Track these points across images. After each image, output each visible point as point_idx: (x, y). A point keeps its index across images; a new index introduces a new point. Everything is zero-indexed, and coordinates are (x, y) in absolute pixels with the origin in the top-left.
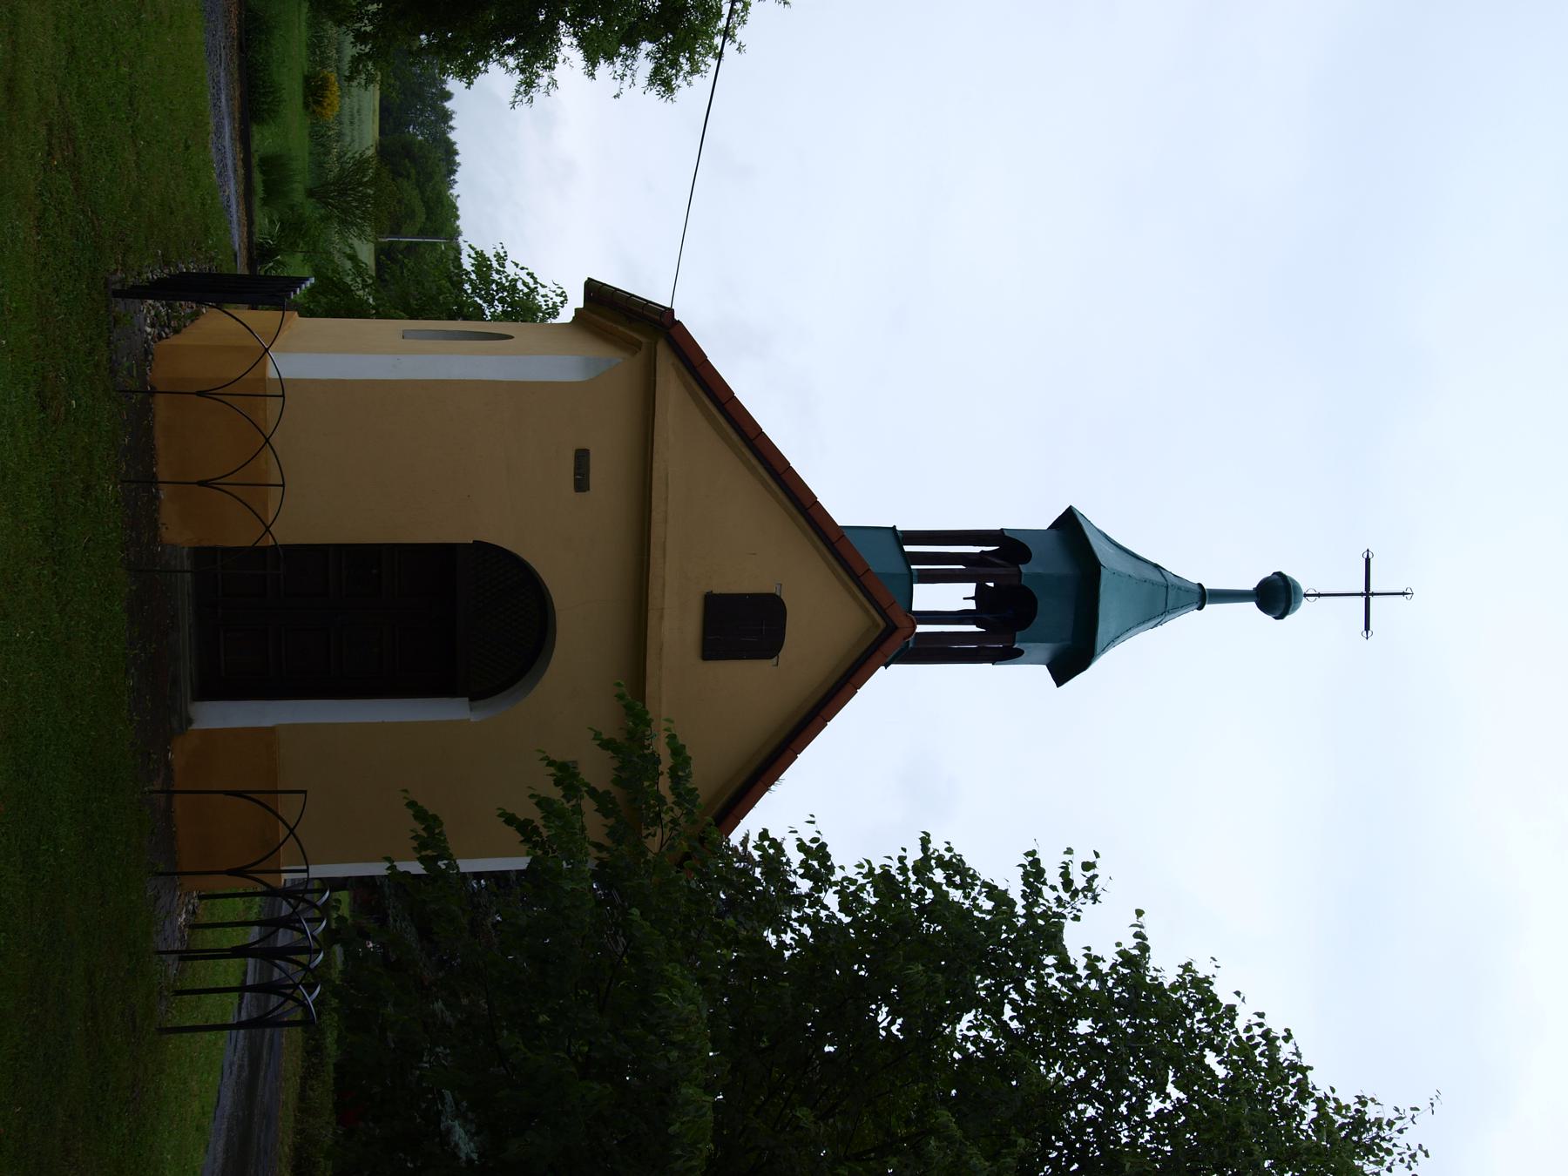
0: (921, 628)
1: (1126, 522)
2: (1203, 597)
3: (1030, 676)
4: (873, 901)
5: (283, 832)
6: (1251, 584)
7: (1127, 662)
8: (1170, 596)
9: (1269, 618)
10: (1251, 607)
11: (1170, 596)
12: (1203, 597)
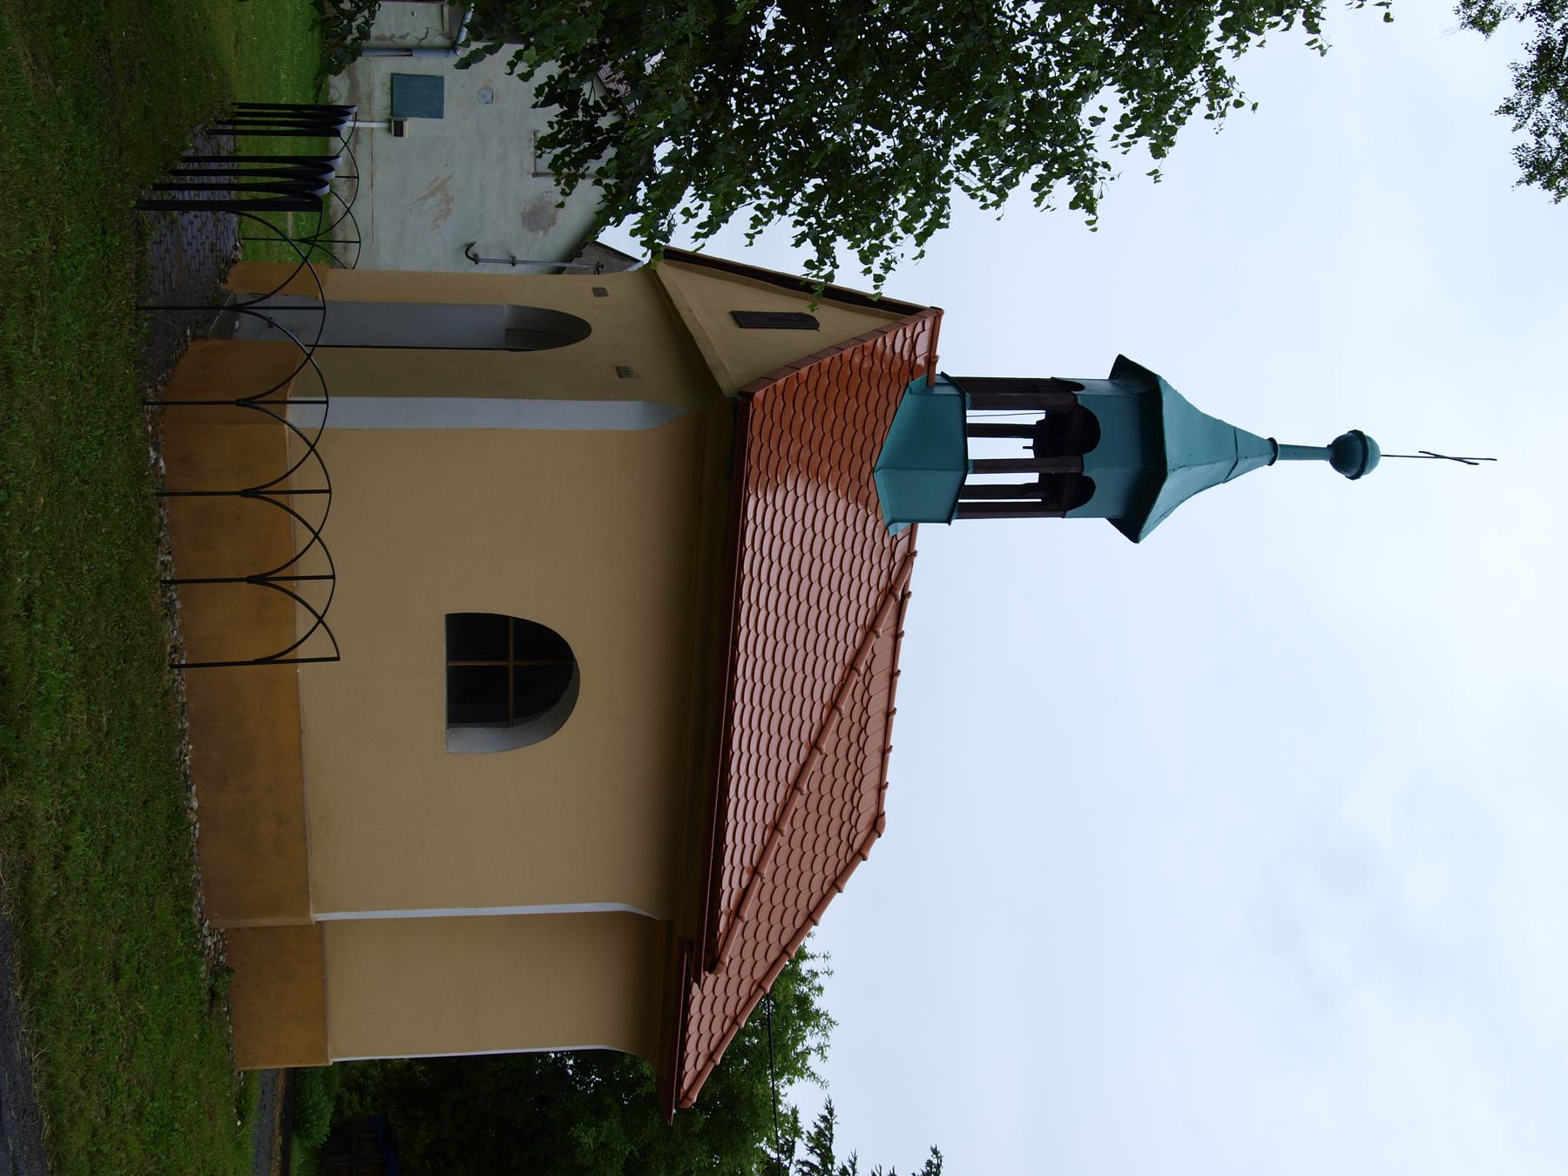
0: (973, 479)
1: (1199, 383)
2: (1275, 451)
3: (1088, 535)
4: (642, 185)
5: (304, 621)
6: (1325, 441)
7: (1192, 520)
8: (1238, 452)
9: (1341, 477)
10: (1325, 466)
11: (1238, 452)
12: (1275, 451)
